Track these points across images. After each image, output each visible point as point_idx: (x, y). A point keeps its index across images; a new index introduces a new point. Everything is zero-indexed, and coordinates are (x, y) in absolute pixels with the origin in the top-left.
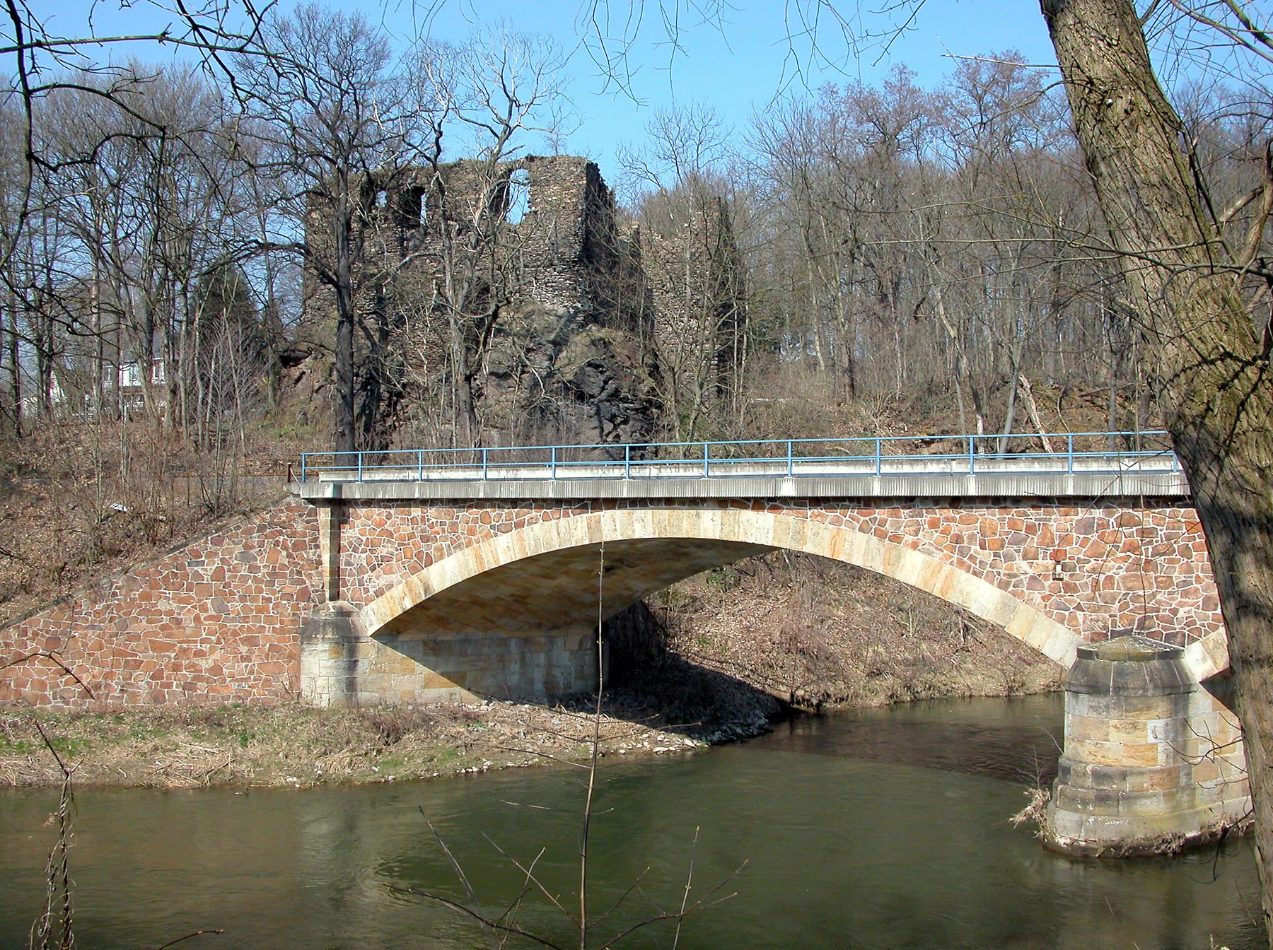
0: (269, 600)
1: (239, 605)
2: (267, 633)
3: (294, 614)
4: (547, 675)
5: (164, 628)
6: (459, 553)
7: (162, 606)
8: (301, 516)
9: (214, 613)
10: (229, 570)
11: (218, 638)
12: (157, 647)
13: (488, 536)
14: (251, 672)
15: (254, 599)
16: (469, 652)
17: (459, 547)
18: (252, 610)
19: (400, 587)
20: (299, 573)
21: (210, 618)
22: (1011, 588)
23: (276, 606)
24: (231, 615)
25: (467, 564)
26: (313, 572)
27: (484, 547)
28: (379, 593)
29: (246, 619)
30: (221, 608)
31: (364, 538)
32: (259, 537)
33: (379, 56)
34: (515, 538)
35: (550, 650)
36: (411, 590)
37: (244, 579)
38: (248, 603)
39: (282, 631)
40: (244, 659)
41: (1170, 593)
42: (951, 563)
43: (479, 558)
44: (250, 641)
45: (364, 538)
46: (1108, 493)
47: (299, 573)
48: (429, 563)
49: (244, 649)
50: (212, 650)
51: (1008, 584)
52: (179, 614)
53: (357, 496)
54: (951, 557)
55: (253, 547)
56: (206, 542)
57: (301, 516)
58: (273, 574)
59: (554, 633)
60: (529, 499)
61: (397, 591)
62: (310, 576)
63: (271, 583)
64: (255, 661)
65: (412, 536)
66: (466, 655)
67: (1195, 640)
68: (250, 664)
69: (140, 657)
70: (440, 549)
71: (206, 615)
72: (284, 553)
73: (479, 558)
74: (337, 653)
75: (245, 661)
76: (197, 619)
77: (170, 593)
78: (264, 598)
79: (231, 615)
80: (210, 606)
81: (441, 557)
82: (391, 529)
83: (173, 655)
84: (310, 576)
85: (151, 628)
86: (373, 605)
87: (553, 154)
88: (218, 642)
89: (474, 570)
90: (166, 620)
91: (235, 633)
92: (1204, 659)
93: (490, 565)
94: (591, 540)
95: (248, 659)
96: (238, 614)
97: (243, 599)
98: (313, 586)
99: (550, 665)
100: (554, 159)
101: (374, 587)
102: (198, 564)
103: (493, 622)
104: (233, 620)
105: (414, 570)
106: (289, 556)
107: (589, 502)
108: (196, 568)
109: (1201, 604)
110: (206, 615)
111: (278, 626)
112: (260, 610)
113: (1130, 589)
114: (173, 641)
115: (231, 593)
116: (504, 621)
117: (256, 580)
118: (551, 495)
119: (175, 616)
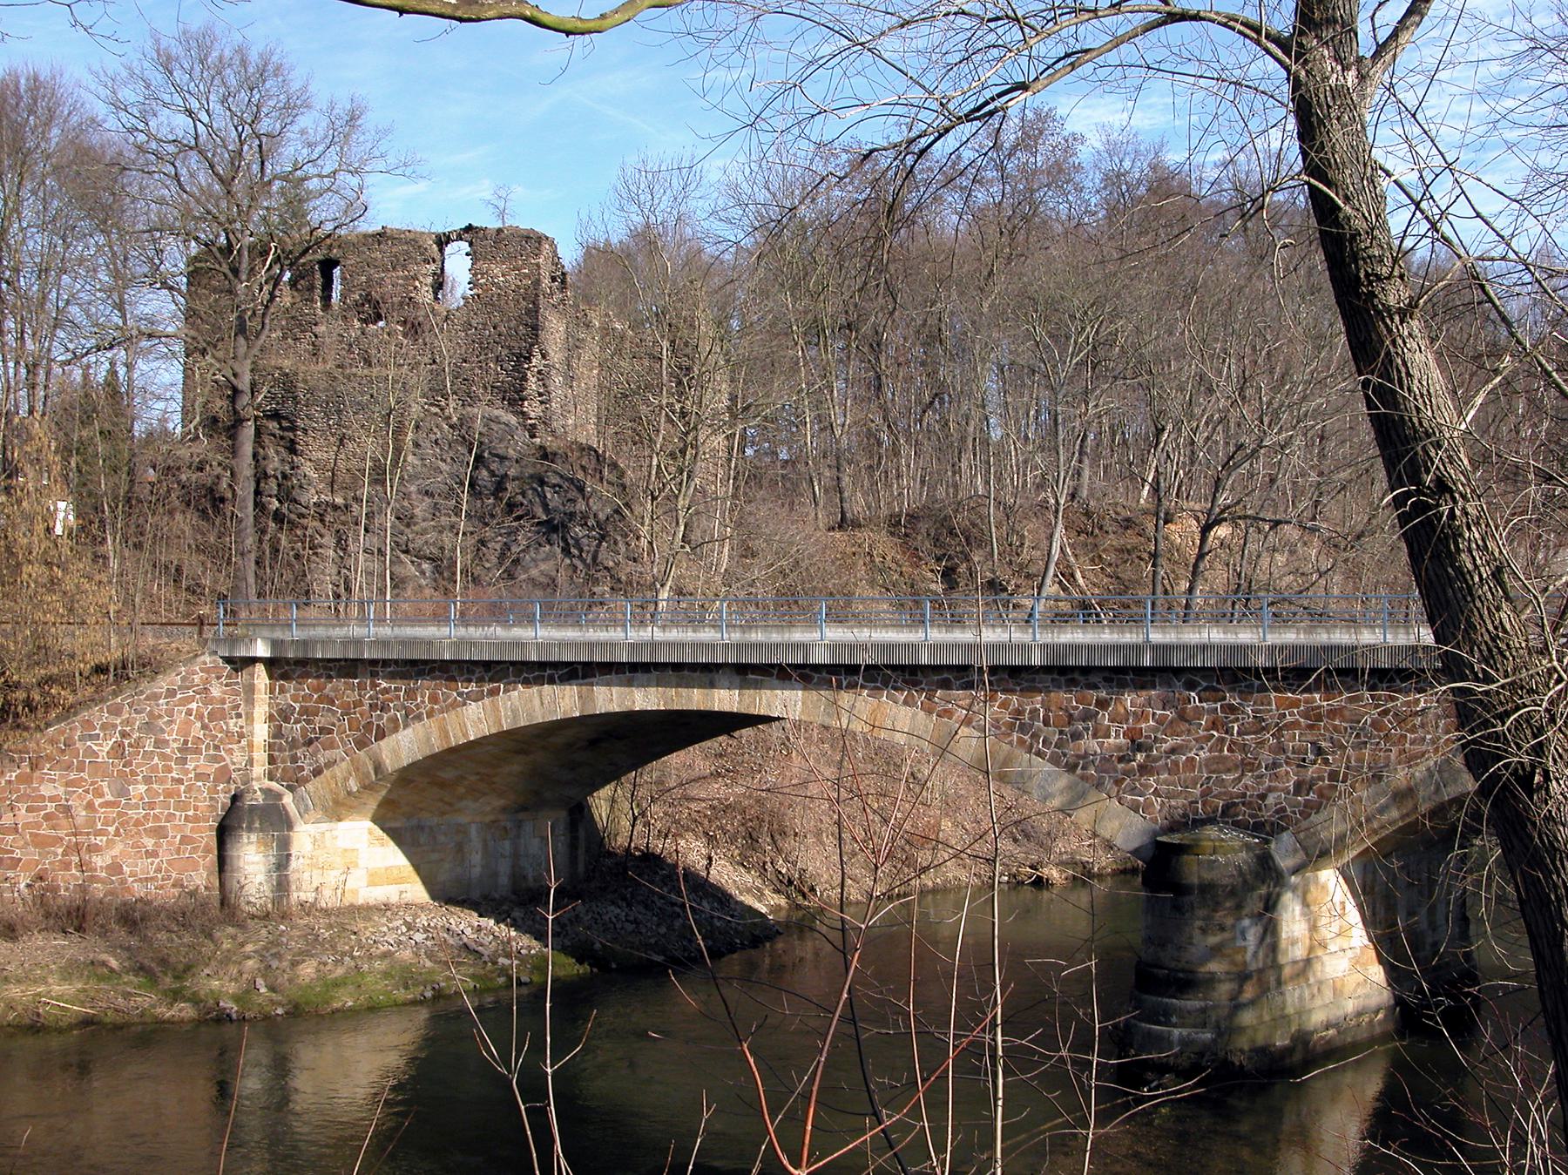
0: (180, 781)
1: (142, 788)
2: (177, 822)
3: (211, 799)
4: (513, 867)
5: (48, 817)
6: (418, 725)
7: (46, 790)
8: (218, 678)
9: (112, 799)
10: (130, 745)
11: (117, 829)
12: (41, 842)
13: (454, 705)
14: (159, 870)
15: (162, 781)
16: (422, 840)
17: (419, 718)
18: (159, 794)
19: (344, 765)
20: (217, 748)
21: (107, 804)
22: (1079, 771)
23: (189, 789)
24: (134, 801)
25: (428, 739)
26: (235, 746)
27: (451, 717)
28: (317, 772)
29: (152, 806)
30: (123, 792)
31: (297, 706)
32: (167, 704)
33: (290, 109)
34: (488, 708)
35: (518, 836)
36: (357, 769)
37: (148, 756)
38: (155, 786)
39: (196, 819)
40: (149, 854)
41: (1258, 777)
42: (1011, 743)
43: (445, 734)
44: (159, 833)
45: (297, 706)
46: (1190, 664)
47: (217, 748)
48: (381, 735)
49: (149, 843)
50: (110, 843)
51: (1076, 766)
52: (67, 801)
53: (290, 655)
54: (1009, 735)
55: (160, 716)
56: (101, 710)
57: (218, 678)
58: (184, 749)
59: (521, 816)
60: (505, 662)
61: (339, 770)
62: (230, 752)
63: (183, 761)
64: (164, 857)
65: (358, 704)
66: (419, 845)
67: (1284, 829)
68: (157, 861)
69: (18, 854)
70: (395, 720)
71: (100, 800)
72: (199, 725)
73: (445, 734)
74: (266, 845)
75: (152, 856)
76: (90, 806)
77: (56, 774)
78: (173, 779)
79: (134, 801)
80: (106, 790)
81: (396, 729)
82: (332, 694)
83: (60, 851)
84: (230, 752)
85: (31, 818)
86: (309, 786)
87: (499, 225)
88: (117, 833)
89: (437, 746)
90: (51, 807)
91: (138, 823)
92: (1295, 851)
93: (456, 739)
94: (581, 711)
95: (154, 854)
96: (142, 798)
97: (147, 780)
98: (234, 764)
99: (516, 855)
100: (499, 231)
101: (310, 765)
102: (91, 738)
103: (450, 805)
104: (136, 806)
105: (361, 744)
106: (204, 727)
107: (579, 667)
108: (89, 743)
109: (1291, 788)
110: (100, 800)
111: (190, 813)
112: (168, 794)
113: (1213, 772)
114: (61, 833)
115: (133, 773)
116: (463, 803)
117: (164, 757)
118: (534, 658)
119: (63, 802)
